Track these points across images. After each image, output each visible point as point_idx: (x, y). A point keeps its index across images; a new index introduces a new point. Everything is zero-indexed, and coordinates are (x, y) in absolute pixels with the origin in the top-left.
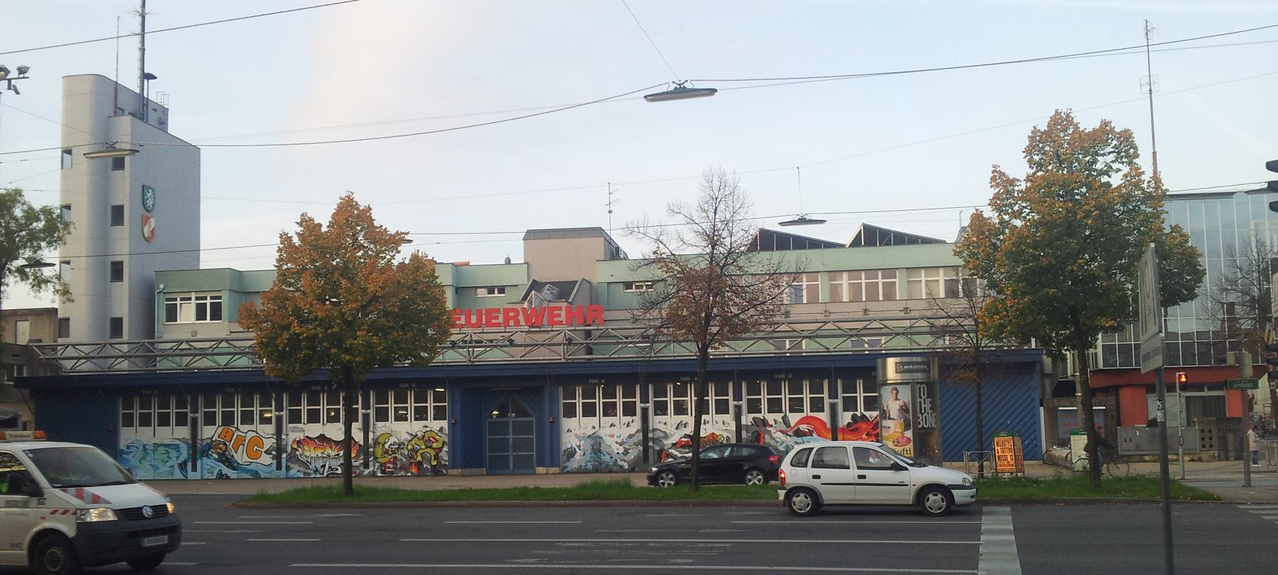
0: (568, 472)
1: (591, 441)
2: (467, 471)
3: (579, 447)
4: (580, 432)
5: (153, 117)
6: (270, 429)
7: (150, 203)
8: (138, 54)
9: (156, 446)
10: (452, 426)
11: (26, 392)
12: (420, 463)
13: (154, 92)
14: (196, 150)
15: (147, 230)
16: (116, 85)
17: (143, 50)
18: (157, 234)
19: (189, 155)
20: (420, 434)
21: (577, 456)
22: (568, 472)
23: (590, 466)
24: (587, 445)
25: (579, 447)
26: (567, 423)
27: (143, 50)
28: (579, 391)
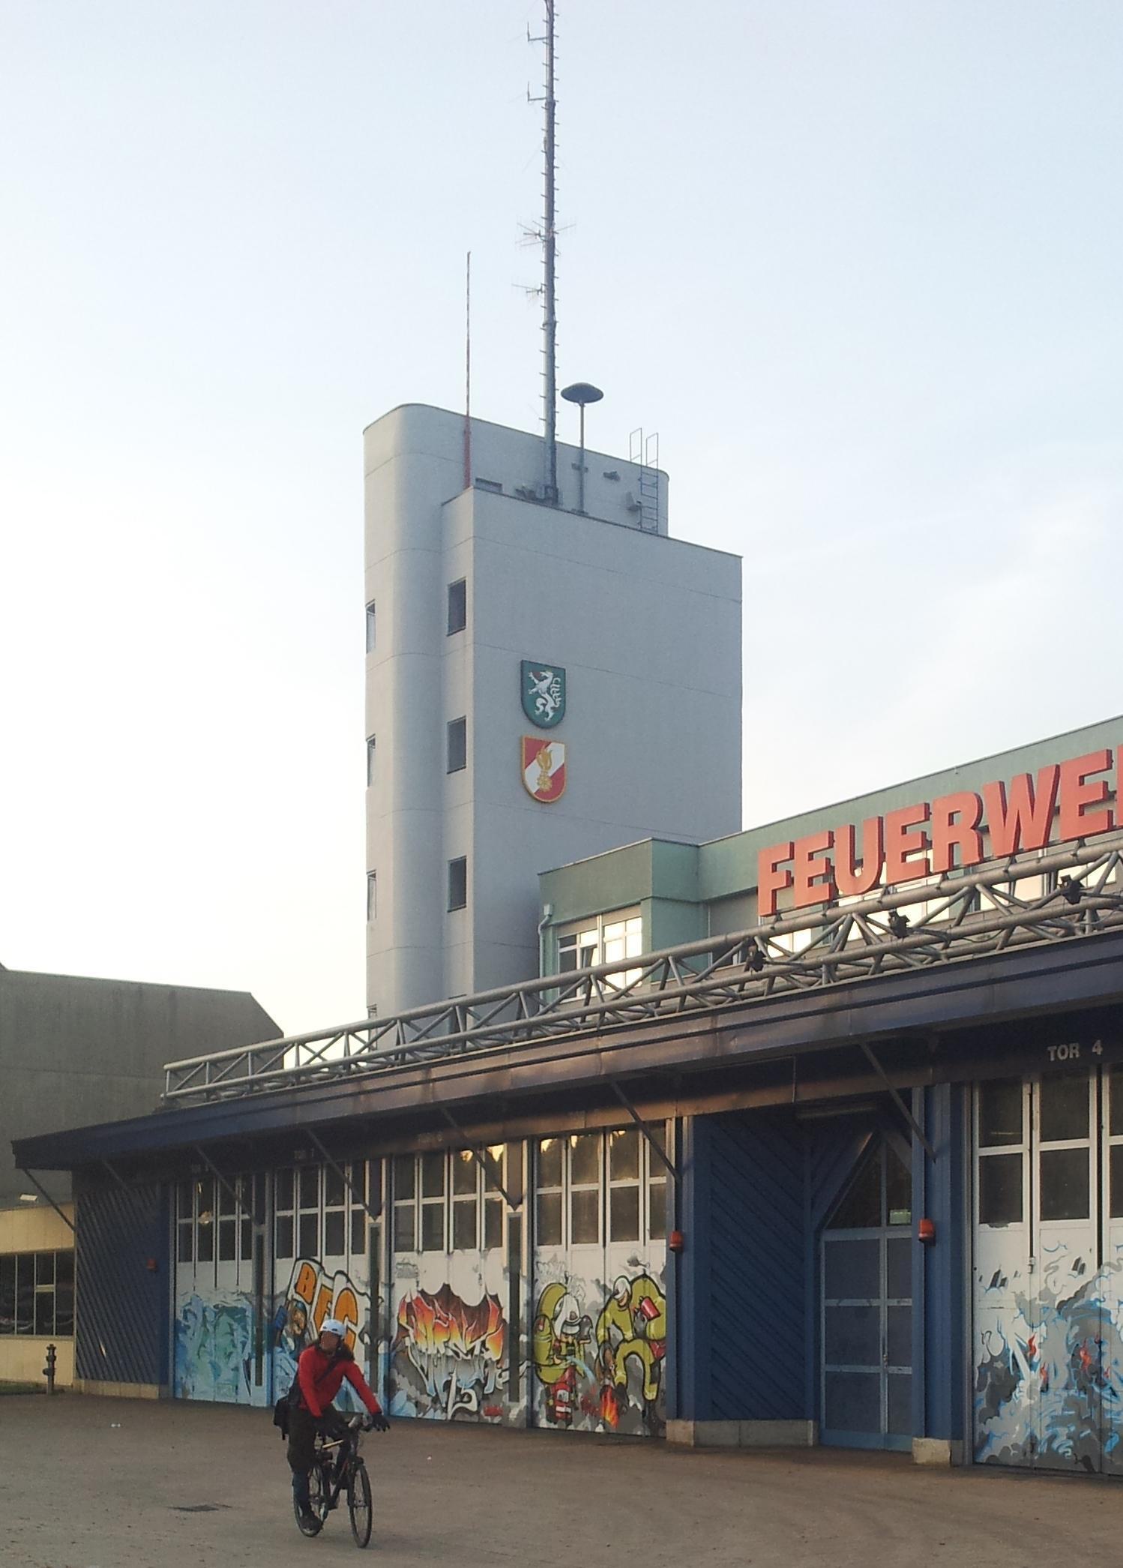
0: (998, 1467)
1: (1066, 1330)
2: (725, 1431)
3: (1029, 1350)
4: (1032, 1292)
5: (603, 498)
6: (359, 1266)
7: (547, 705)
8: (541, 337)
9: (220, 1310)
10: (676, 1252)
11: (61, 1180)
12: (621, 1391)
13: (601, 433)
14: (734, 561)
15: (534, 776)
16: (467, 426)
17: (551, 326)
18: (569, 783)
19: (718, 576)
20: (623, 1287)
21: (1024, 1395)
22: (998, 1467)
23: (1064, 1445)
24: (1053, 1344)
25: (1029, 1350)
26: (184, 1271)
27: (551, 326)
28: (1031, 1105)
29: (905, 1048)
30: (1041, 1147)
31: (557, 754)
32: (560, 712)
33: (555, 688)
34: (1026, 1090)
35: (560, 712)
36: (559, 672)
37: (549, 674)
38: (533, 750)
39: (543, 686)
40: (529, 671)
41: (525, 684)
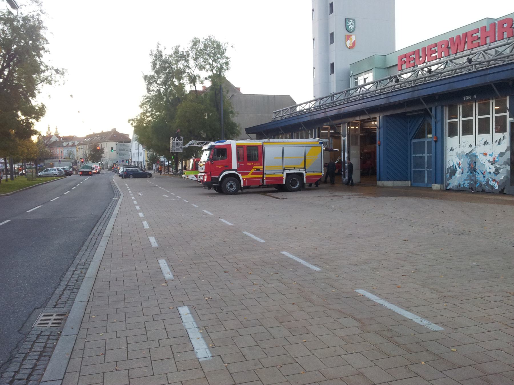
7: (351, 27)
15: (349, 43)
29: (431, 99)
30: (462, 119)
31: (354, 38)
32: (354, 28)
33: (353, 23)
34: (458, 106)
35: (354, 28)
36: (354, 20)
37: (352, 21)
38: (348, 37)
39: (350, 23)
40: (347, 20)
41: (346, 23)
